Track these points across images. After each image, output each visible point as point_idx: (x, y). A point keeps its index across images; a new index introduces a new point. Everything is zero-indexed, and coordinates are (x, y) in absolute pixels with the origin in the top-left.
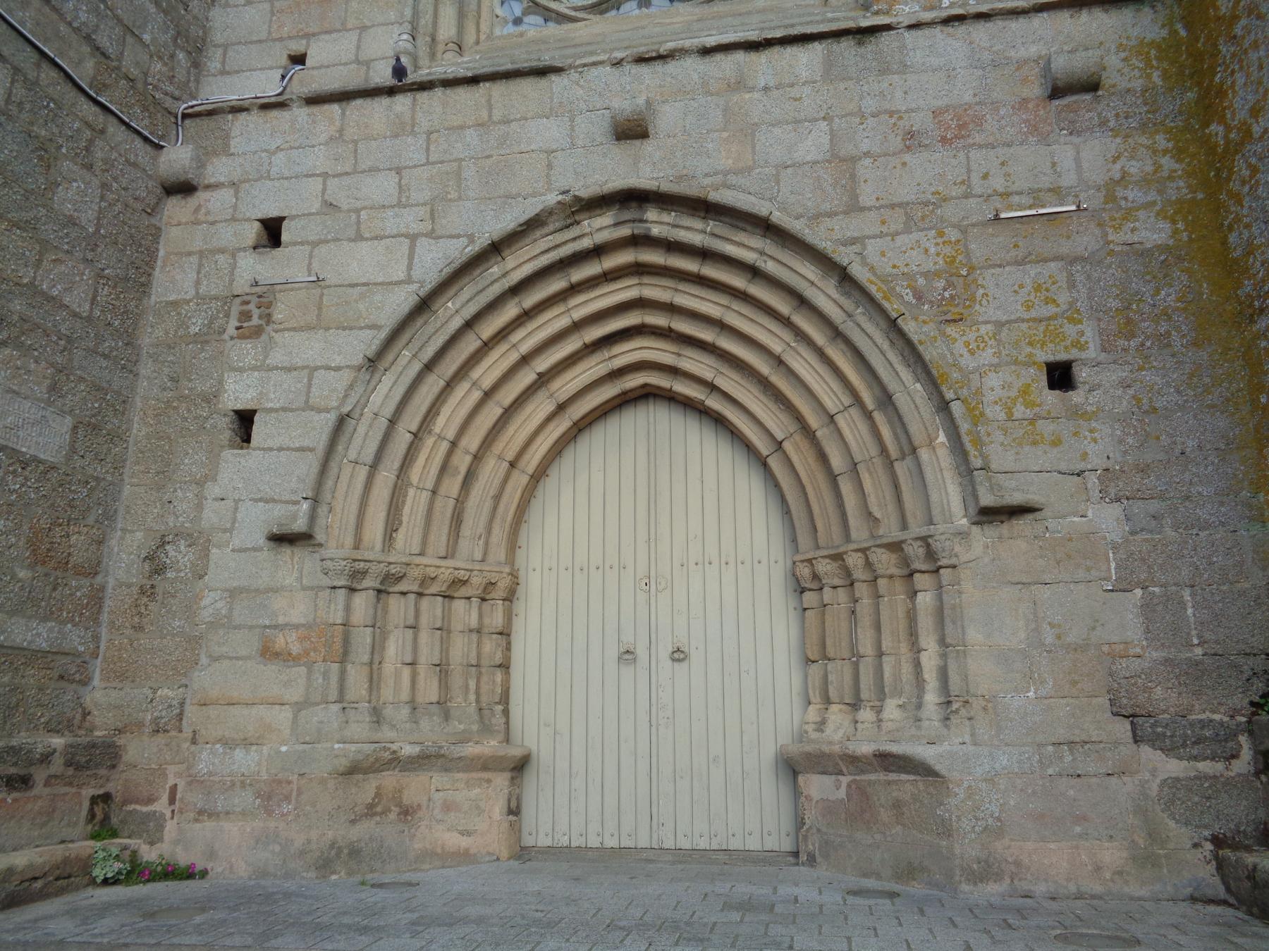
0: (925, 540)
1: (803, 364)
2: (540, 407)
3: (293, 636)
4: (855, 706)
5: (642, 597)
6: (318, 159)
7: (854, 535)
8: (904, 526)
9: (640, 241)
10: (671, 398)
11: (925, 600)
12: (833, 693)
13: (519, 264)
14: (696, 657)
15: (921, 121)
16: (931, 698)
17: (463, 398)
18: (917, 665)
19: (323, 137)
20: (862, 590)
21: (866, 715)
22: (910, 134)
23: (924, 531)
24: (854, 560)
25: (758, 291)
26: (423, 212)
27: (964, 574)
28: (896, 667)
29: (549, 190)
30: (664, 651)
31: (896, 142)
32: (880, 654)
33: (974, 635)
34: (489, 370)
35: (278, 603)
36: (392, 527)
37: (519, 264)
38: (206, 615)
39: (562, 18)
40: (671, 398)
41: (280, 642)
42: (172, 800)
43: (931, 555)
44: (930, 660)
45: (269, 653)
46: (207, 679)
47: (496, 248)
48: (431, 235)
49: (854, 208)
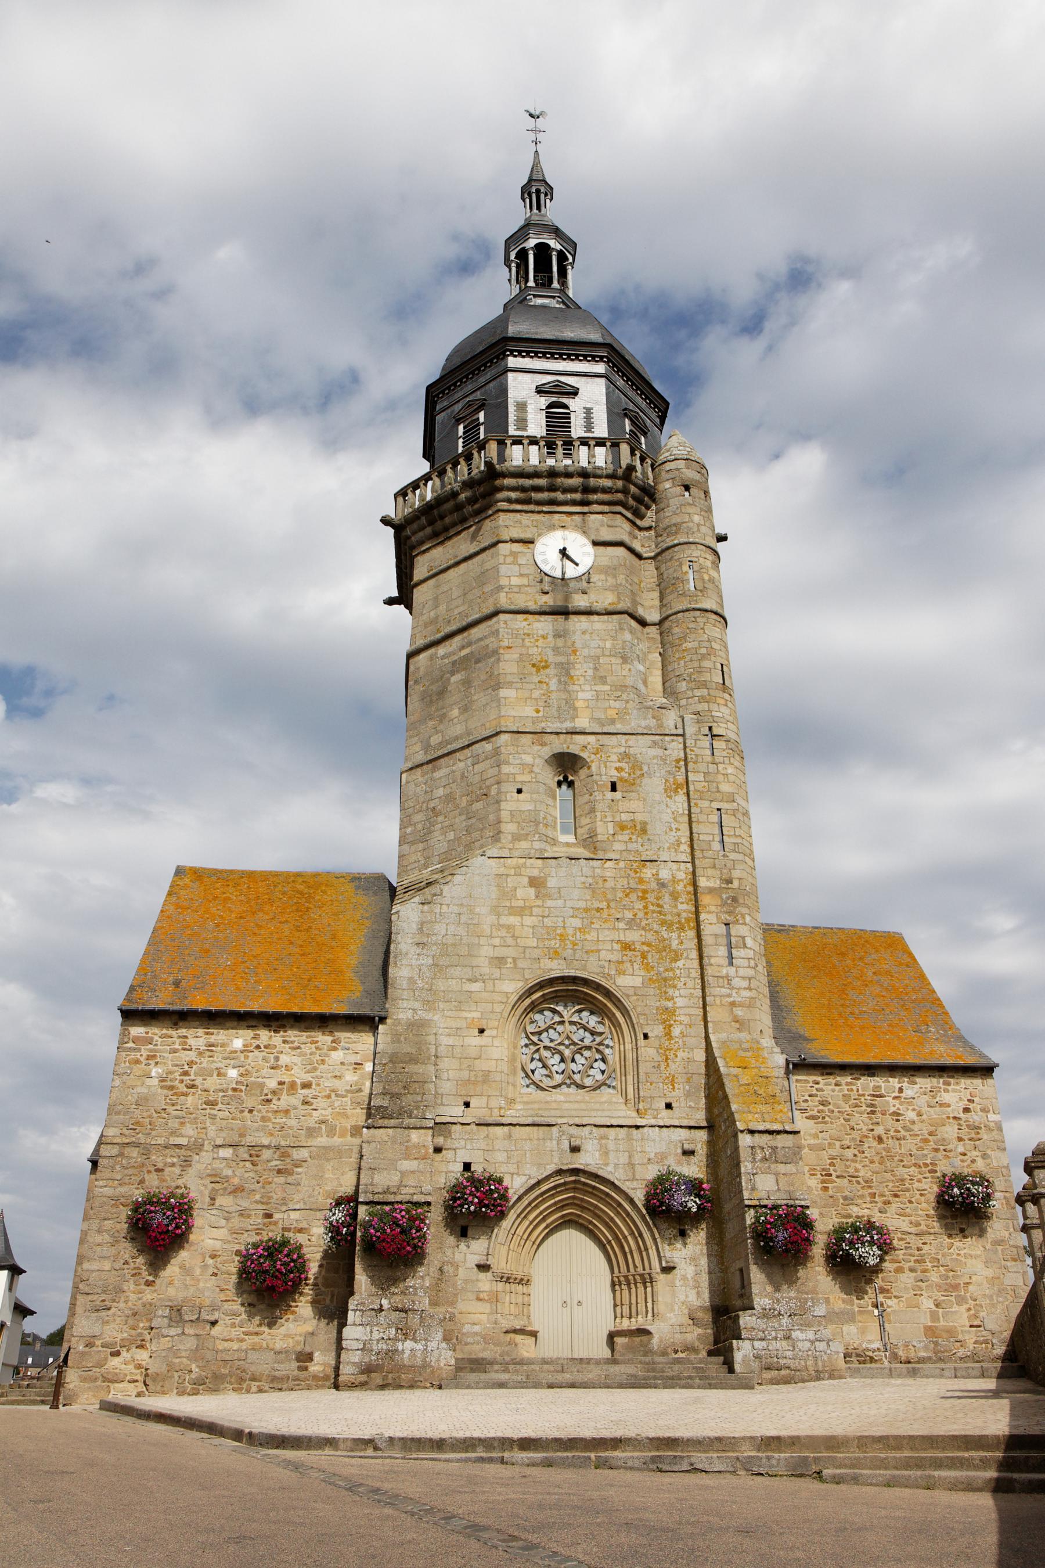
0: (649, 1274)
1: (629, 1238)
2: (543, 1225)
3: (485, 1294)
4: (630, 1317)
5: (569, 1285)
6: (482, 1144)
7: (622, 1271)
8: (644, 1270)
9: (579, 1182)
10: (577, 1223)
11: (649, 1289)
12: (624, 1314)
13: (545, 1187)
14: (584, 1304)
15: (652, 1155)
16: (650, 1314)
17: (526, 1223)
18: (646, 1307)
19: (482, 1137)
20: (633, 1286)
21: (633, 1320)
22: (649, 1160)
23: (649, 1271)
24: (631, 1278)
25: (644, 1254)
26: (515, 1166)
27: (658, 1283)
28: (641, 1307)
29: (552, 1163)
30: (575, 1302)
31: (646, 1161)
32: (637, 1303)
33: (660, 1299)
34: (531, 1217)
35: (480, 1284)
36: (635, 1267)
37: (545, 1187)
38: (459, 1287)
39: (543, 1089)
40: (577, 1223)
41: (481, 1296)
42: (457, 1339)
43: (651, 1278)
44: (650, 1305)
45: (479, 1299)
46: (461, 1306)
47: (539, 1183)
48: (518, 1174)
49: (634, 1179)
